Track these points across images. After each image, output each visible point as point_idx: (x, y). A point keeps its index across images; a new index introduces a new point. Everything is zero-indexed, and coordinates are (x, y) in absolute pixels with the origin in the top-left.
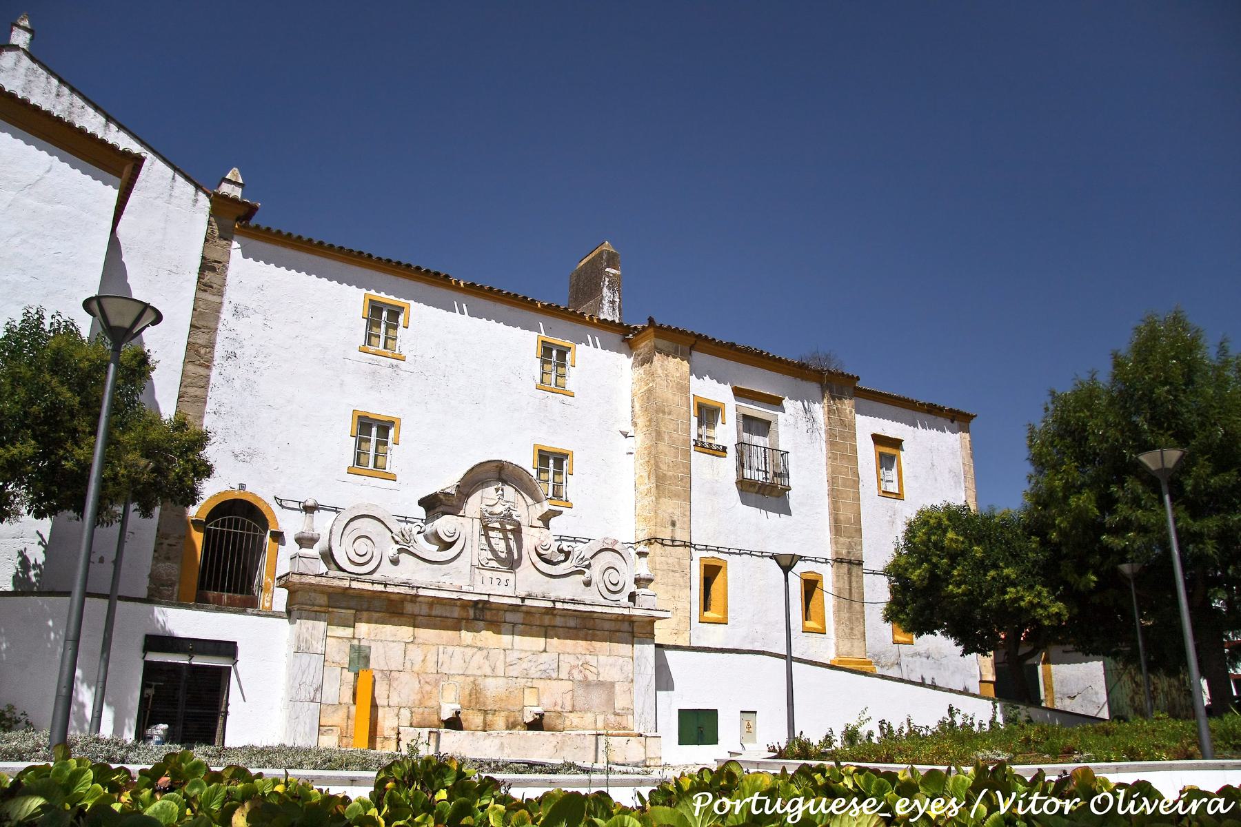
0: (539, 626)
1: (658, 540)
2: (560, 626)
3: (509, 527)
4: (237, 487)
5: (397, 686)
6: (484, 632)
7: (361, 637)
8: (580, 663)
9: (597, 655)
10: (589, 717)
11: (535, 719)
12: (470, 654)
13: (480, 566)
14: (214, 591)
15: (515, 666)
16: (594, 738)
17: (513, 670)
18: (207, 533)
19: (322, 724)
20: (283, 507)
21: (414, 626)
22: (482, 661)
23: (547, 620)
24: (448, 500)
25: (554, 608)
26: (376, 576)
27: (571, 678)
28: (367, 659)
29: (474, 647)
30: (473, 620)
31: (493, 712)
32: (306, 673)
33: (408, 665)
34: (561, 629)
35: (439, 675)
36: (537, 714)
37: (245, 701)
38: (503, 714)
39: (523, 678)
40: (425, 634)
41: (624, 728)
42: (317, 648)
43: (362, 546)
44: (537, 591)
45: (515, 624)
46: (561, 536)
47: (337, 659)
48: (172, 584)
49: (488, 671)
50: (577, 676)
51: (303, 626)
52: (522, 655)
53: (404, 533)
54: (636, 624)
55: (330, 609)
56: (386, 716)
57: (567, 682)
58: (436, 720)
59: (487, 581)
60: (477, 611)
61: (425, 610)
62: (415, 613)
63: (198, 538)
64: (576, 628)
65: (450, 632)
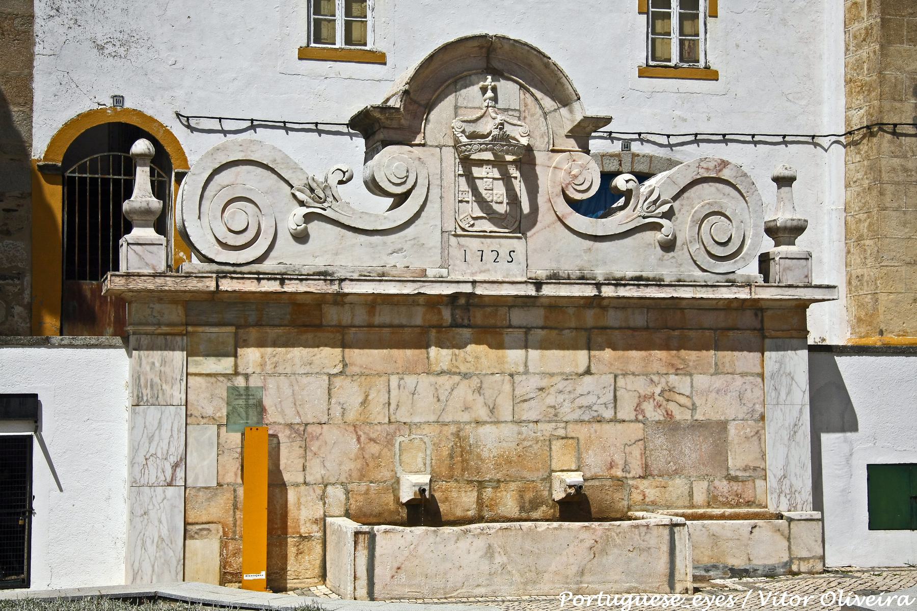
0: (576, 329)
1: (885, 128)
2: (617, 325)
3: (509, 158)
4: (109, 103)
5: (319, 449)
6: (471, 348)
7: (250, 371)
8: (658, 390)
9: (691, 375)
10: (678, 485)
11: (568, 495)
12: (448, 386)
13: (459, 232)
14: (91, 279)
15: (532, 402)
16: (666, 532)
17: (530, 409)
18: (68, 184)
19: (190, 521)
20: (193, 129)
21: (344, 345)
22: (470, 397)
23: (590, 317)
24: (392, 120)
25: (598, 297)
26: (268, 266)
27: (640, 417)
28: (261, 409)
29: (455, 373)
30: (451, 326)
31: (494, 484)
32: (156, 438)
33: (336, 411)
34: (617, 332)
35: (393, 427)
36: (570, 487)
37: (61, 490)
38: (513, 486)
39: (549, 422)
40: (360, 357)
41: (749, 504)
42: (172, 396)
43: (239, 216)
44: (569, 267)
45: (528, 329)
46: (696, 135)
47: (209, 411)
48: (19, 274)
49: (483, 414)
50: (653, 413)
51: (144, 362)
52: (544, 383)
53: (314, 185)
54: (769, 313)
55: (190, 329)
56: (303, 500)
57: (632, 425)
58: (392, 503)
59: (473, 257)
60: (458, 311)
61: (361, 317)
62: (344, 323)
63: (54, 195)
64: (647, 328)
65: (409, 352)
